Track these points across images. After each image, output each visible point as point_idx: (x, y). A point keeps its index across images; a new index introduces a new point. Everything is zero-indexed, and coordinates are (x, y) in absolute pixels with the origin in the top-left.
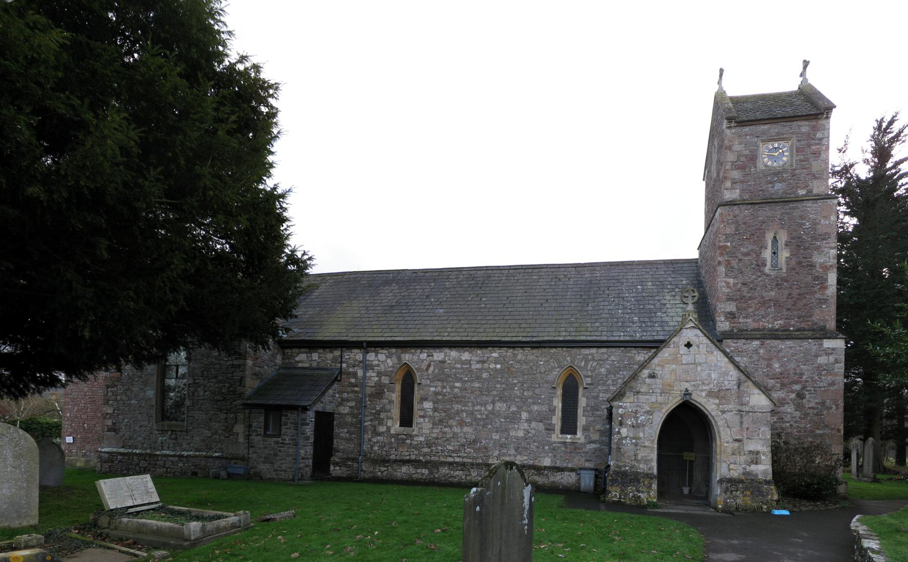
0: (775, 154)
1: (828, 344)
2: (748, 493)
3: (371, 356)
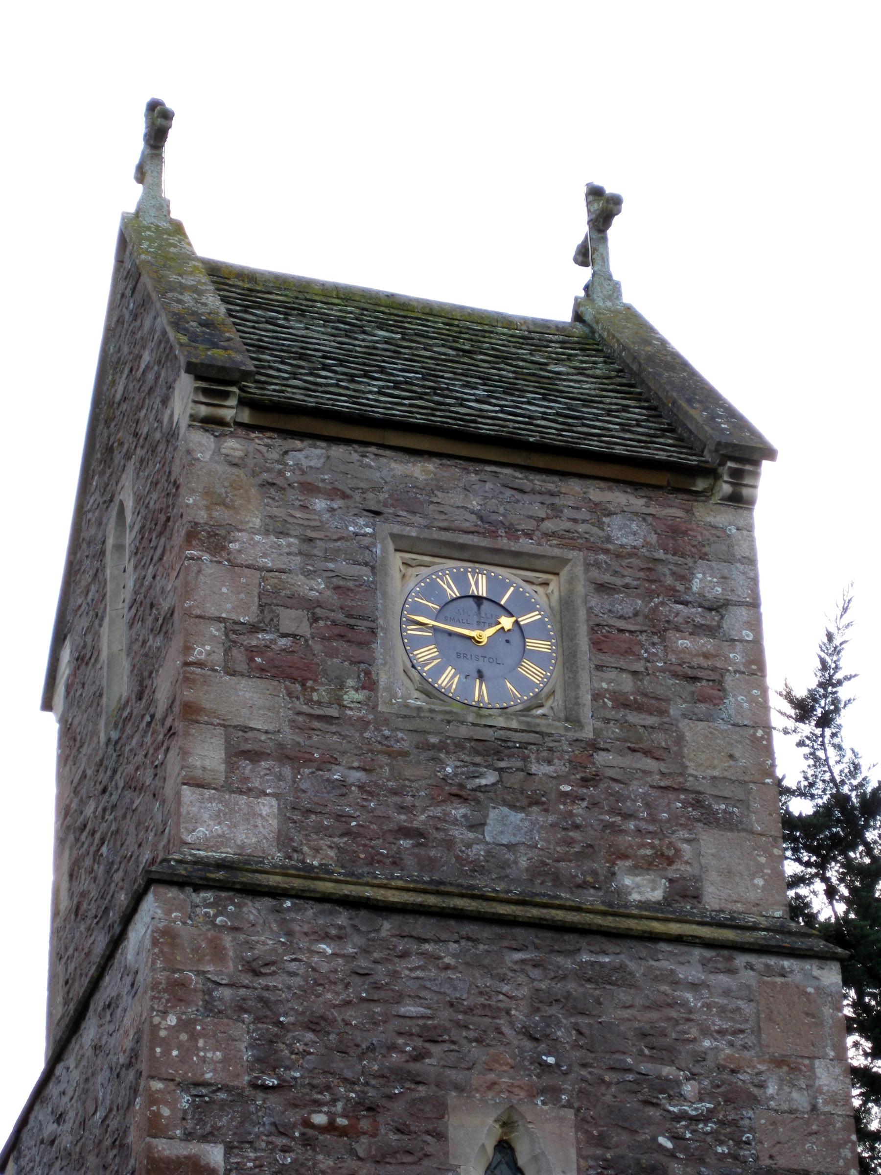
0: (475, 633)
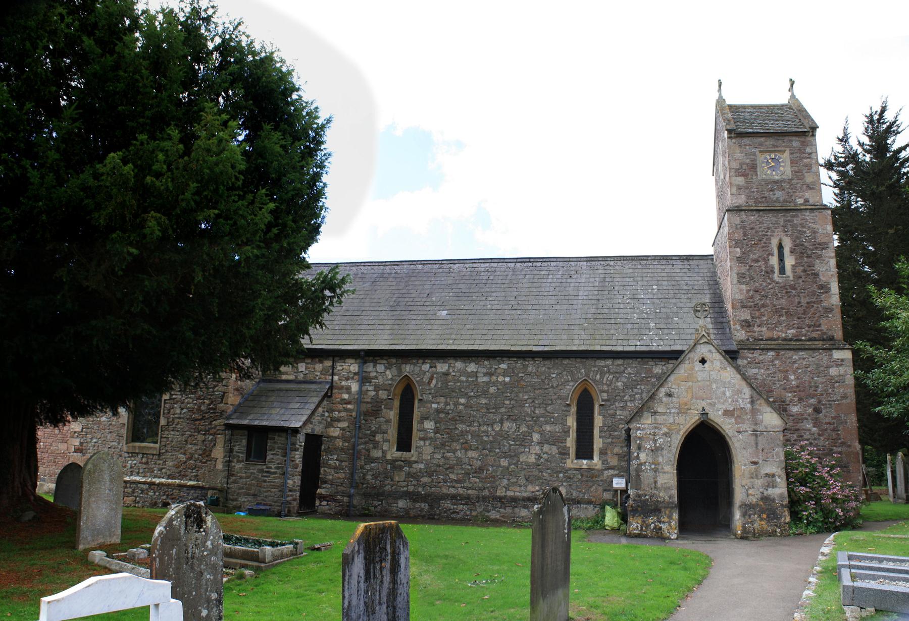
1: (837, 355)
2: (764, 516)
3: (369, 367)
